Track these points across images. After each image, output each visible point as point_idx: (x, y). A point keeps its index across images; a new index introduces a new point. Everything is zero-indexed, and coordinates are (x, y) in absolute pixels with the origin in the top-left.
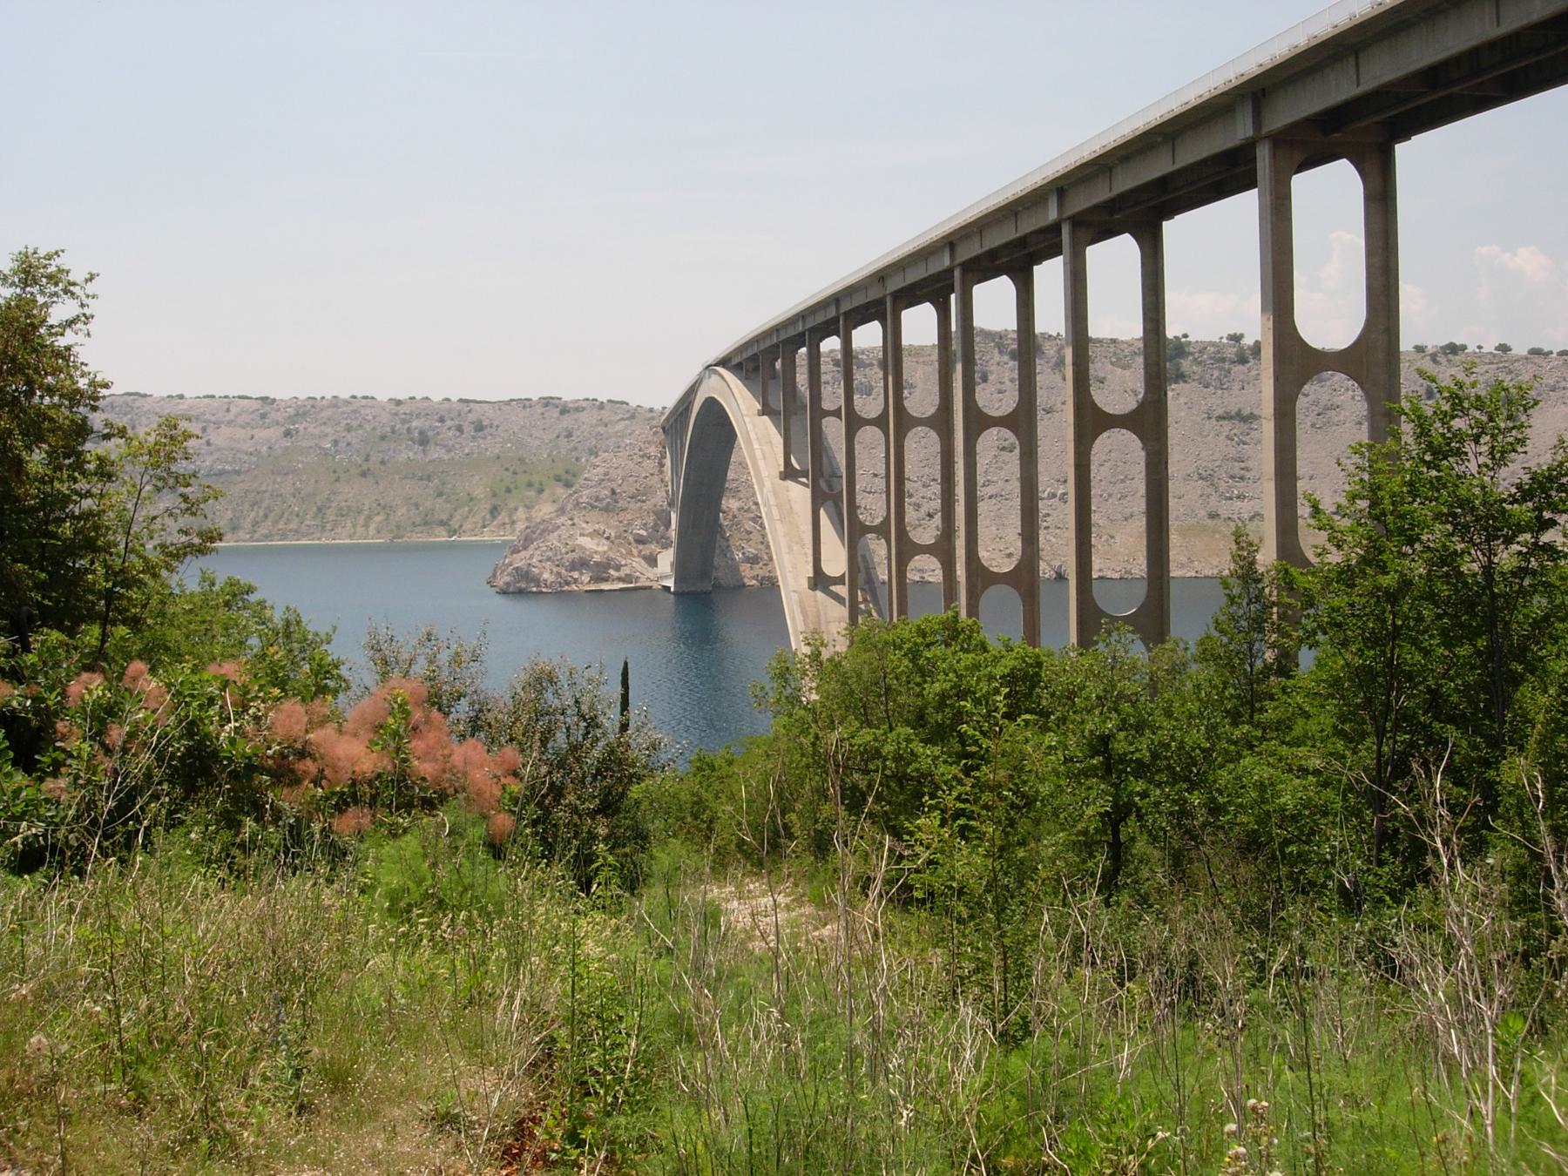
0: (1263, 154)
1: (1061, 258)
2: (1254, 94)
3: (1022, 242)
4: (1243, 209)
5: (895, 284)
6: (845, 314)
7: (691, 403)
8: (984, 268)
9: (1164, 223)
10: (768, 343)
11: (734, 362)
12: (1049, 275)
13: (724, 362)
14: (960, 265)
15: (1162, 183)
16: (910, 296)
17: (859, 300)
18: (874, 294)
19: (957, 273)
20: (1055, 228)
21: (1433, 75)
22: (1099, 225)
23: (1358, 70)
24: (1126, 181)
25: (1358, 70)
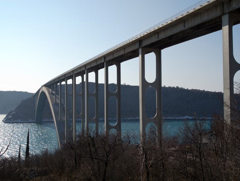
0: (140, 51)
1: (104, 69)
2: (139, 41)
3: (97, 66)
4: (137, 61)
5: (75, 72)
6: (66, 78)
7: (39, 92)
8: (90, 70)
9: (162, 50)
10: (50, 84)
11: (47, 85)
12: (102, 72)
13: (45, 85)
14: (106, 62)
15: (122, 56)
16: (77, 75)
17: (69, 75)
18: (71, 74)
19: (105, 63)
20: (103, 64)
21: (170, 37)
22: (110, 63)
23: (223, 8)
24: (116, 56)
25: (223, 8)
